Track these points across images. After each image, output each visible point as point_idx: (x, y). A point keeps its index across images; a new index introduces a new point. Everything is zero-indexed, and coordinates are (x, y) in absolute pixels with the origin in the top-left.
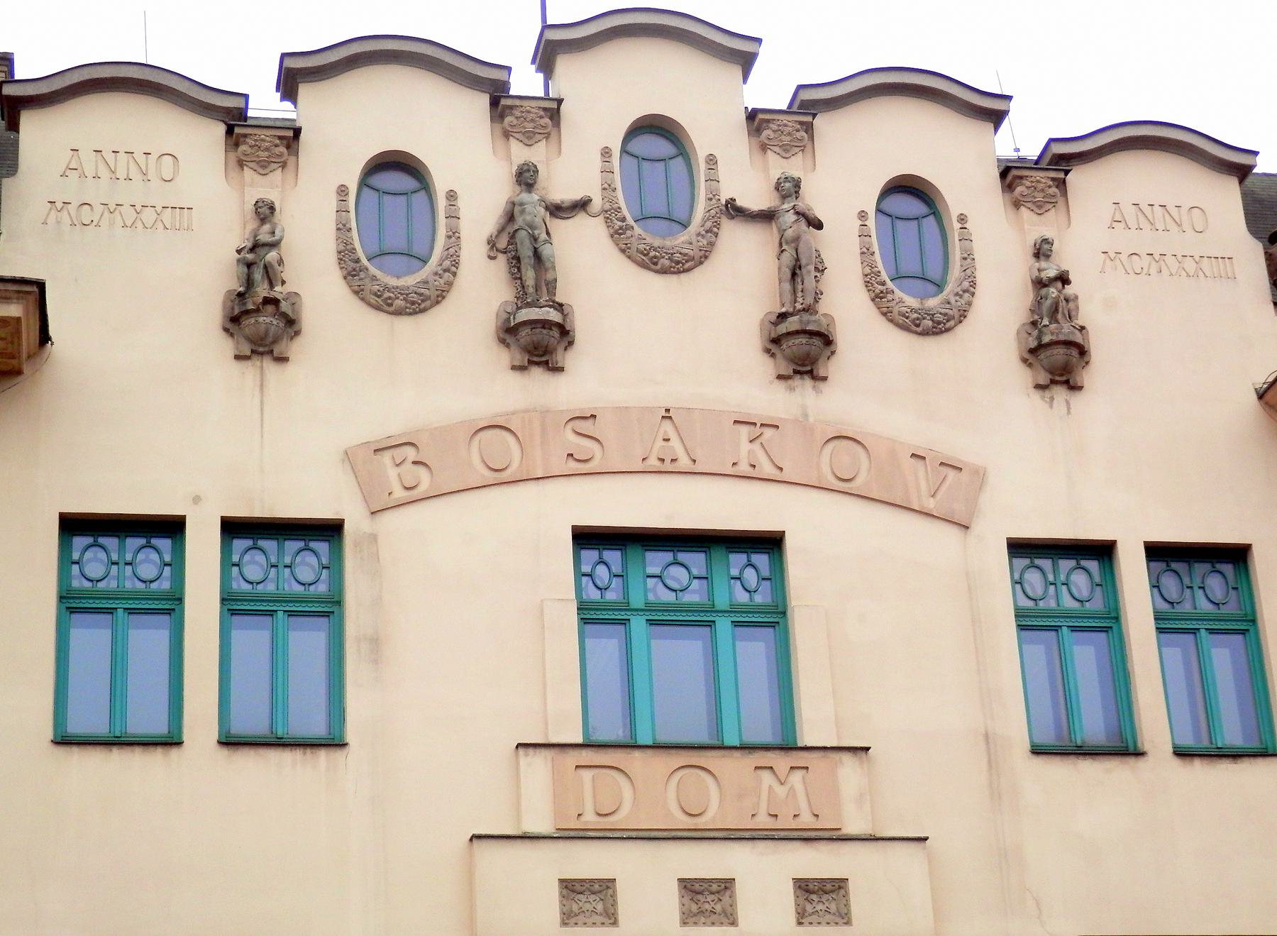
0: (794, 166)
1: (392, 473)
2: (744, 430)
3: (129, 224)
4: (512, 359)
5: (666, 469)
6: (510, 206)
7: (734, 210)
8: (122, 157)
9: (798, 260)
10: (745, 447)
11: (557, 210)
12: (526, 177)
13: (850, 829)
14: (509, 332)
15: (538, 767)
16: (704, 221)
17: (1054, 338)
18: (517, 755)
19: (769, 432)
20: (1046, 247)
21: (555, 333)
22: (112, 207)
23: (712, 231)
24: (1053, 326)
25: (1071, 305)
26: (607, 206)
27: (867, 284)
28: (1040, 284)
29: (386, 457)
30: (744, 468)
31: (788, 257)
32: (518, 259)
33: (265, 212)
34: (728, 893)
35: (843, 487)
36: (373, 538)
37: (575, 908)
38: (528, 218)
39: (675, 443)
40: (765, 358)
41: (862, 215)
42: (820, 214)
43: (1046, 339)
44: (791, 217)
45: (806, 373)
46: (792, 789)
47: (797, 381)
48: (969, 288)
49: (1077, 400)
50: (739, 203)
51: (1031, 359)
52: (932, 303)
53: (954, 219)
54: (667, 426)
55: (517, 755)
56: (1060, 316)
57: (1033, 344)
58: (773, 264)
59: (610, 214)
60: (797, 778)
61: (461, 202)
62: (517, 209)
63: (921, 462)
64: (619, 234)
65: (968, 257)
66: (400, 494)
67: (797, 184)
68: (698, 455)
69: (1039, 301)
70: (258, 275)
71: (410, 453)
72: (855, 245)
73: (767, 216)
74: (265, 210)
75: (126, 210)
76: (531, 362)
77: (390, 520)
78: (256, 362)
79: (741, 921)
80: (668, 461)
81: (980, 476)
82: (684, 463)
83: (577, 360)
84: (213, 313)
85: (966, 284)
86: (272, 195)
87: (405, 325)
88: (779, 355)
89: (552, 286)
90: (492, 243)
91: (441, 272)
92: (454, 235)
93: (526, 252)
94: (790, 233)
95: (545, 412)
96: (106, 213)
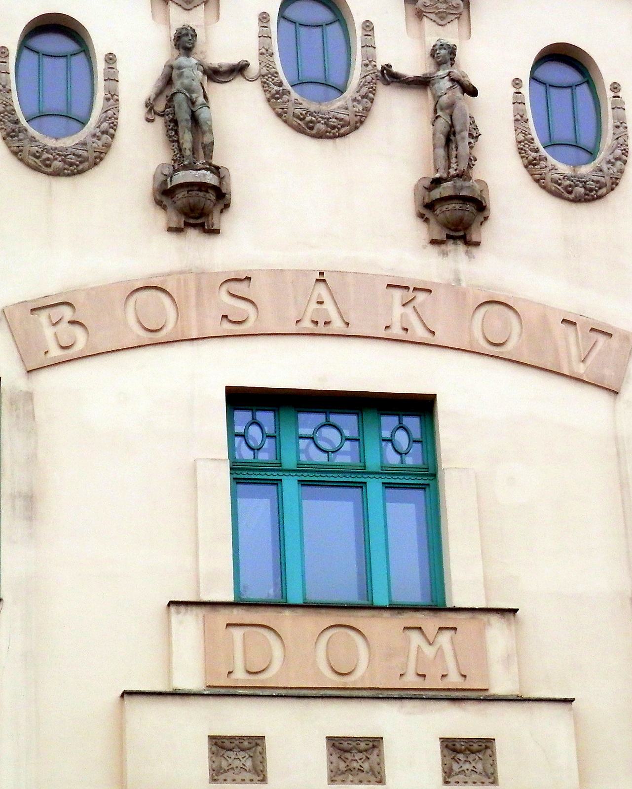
0: (450, 34)
1: (49, 332)
2: (397, 294)
4: (169, 221)
7: (389, 76)
9: (452, 126)
10: (398, 311)
11: (215, 74)
13: (498, 689)
18: (169, 613)
21: (212, 196)
23: (368, 97)
27: (521, 150)
29: (43, 317)
30: (396, 331)
31: (442, 123)
36: (29, 396)
38: (186, 81)
39: (329, 305)
41: (517, 83)
42: (474, 80)
44: (446, 84)
45: (459, 238)
46: (440, 649)
47: (450, 246)
54: (321, 289)
55: (169, 613)
58: (428, 130)
59: (267, 79)
61: (120, 66)
62: (175, 73)
63: (570, 329)
66: (56, 353)
67: (452, 51)
68: (352, 318)
72: (508, 113)
73: (422, 83)
76: (187, 225)
82: (420, 333)
85: (618, 152)
87: (63, 185)
89: (208, 149)
90: (150, 106)
91: (99, 134)
92: (112, 97)
93: (184, 115)
94: (444, 99)
95: (200, 274)
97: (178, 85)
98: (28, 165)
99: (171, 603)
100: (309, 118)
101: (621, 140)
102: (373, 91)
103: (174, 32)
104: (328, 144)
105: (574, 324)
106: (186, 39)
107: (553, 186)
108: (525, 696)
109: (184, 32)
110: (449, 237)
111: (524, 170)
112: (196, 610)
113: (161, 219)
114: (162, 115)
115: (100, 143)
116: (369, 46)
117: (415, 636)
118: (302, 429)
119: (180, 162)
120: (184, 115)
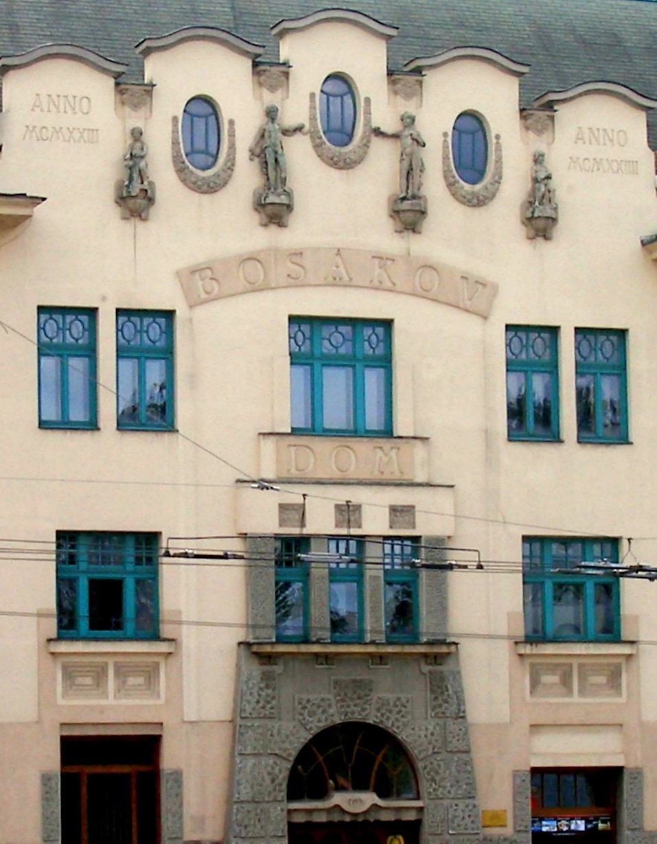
0: (409, 107)
1: (200, 283)
2: (377, 261)
3: (67, 139)
4: (262, 219)
5: (336, 282)
6: (262, 131)
7: (378, 132)
8: (62, 100)
9: (411, 165)
10: (377, 271)
11: (285, 132)
12: (271, 114)
13: (419, 480)
14: (259, 205)
15: (269, 445)
16: (362, 139)
17: (540, 214)
18: (259, 441)
19: (389, 263)
20: (541, 158)
21: (285, 207)
22: (58, 129)
23: (366, 145)
24: (541, 207)
25: (551, 194)
26: (312, 130)
27: (445, 177)
28: (536, 180)
29: (197, 276)
30: (376, 283)
31: (406, 163)
32: (266, 163)
33: (137, 135)
34: (357, 512)
35: (423, 294)
36: (191, 320)
37: (285, 517)
38: (273, 140)
39: (342, 269)
40: (391, 220)
41: (445, 134)
42: (425, 138)
43: (536, 215)
44: (409, 141)
45: (410, 229)
46: (391, 458)
47: (406, 233)
48: (498, 181)
49: (549, 245)
50: (382, 129)
51: (527, 222)
52: (478, 187)
53: (493, 135)
54: (338, 259)
55: (259, 441)
56: (544, 201)
57: (529, 215)
58: (397, 166)
59: (313, 135)
60: (393, 453)
61: (237, 127)
62: (266, 134)
63: (465, 281)
64: (317, 146)
65: (499, 160)
66: (204, 296)
67: (413, 119)
68: (353, 276)
69: (533, 191)
70: (135, 175)
71: (209, 273)
72: (440, 154)
73: (396, 136)
74: (137, 135)
75: (65, 130)
76: (270, 222)
77: (201, 313)
78: (132, 220)
79: (363, 526)
80: (338, 279)
81: (495, 289)
83: (296, 221)
84: (107, 193)
85: (497, 178)
86: (139, 124)
87: (206, 198)
88: (397, 219)
89: (284, 181)
90: (252, 152)
91: (225, 169)
92: (232, 146)
93: (271, 161)
94: (408, 150)
95: (276, 250)
96: (55, 134)
97: (267, 142)
98: (189, 188)
99: (260, 434)
100: (335, 159)
101: (498, 170)
102: (369, 141)
103: (265, 108)
104: (344, 172)
105: (467, 279)
106: (273, 113)
107: (462, 199)
108: (433, 483)
109: (272, 109)
110: (406, 229)
111: (446, 188)
112: (273, 438)
113: (256, 218)
114: (258, 156)
115: (226, 174)
116: (368, 112)
117: (378, 450)
118: (518, 611)
119: (268, 186)
120: (271, 161)
